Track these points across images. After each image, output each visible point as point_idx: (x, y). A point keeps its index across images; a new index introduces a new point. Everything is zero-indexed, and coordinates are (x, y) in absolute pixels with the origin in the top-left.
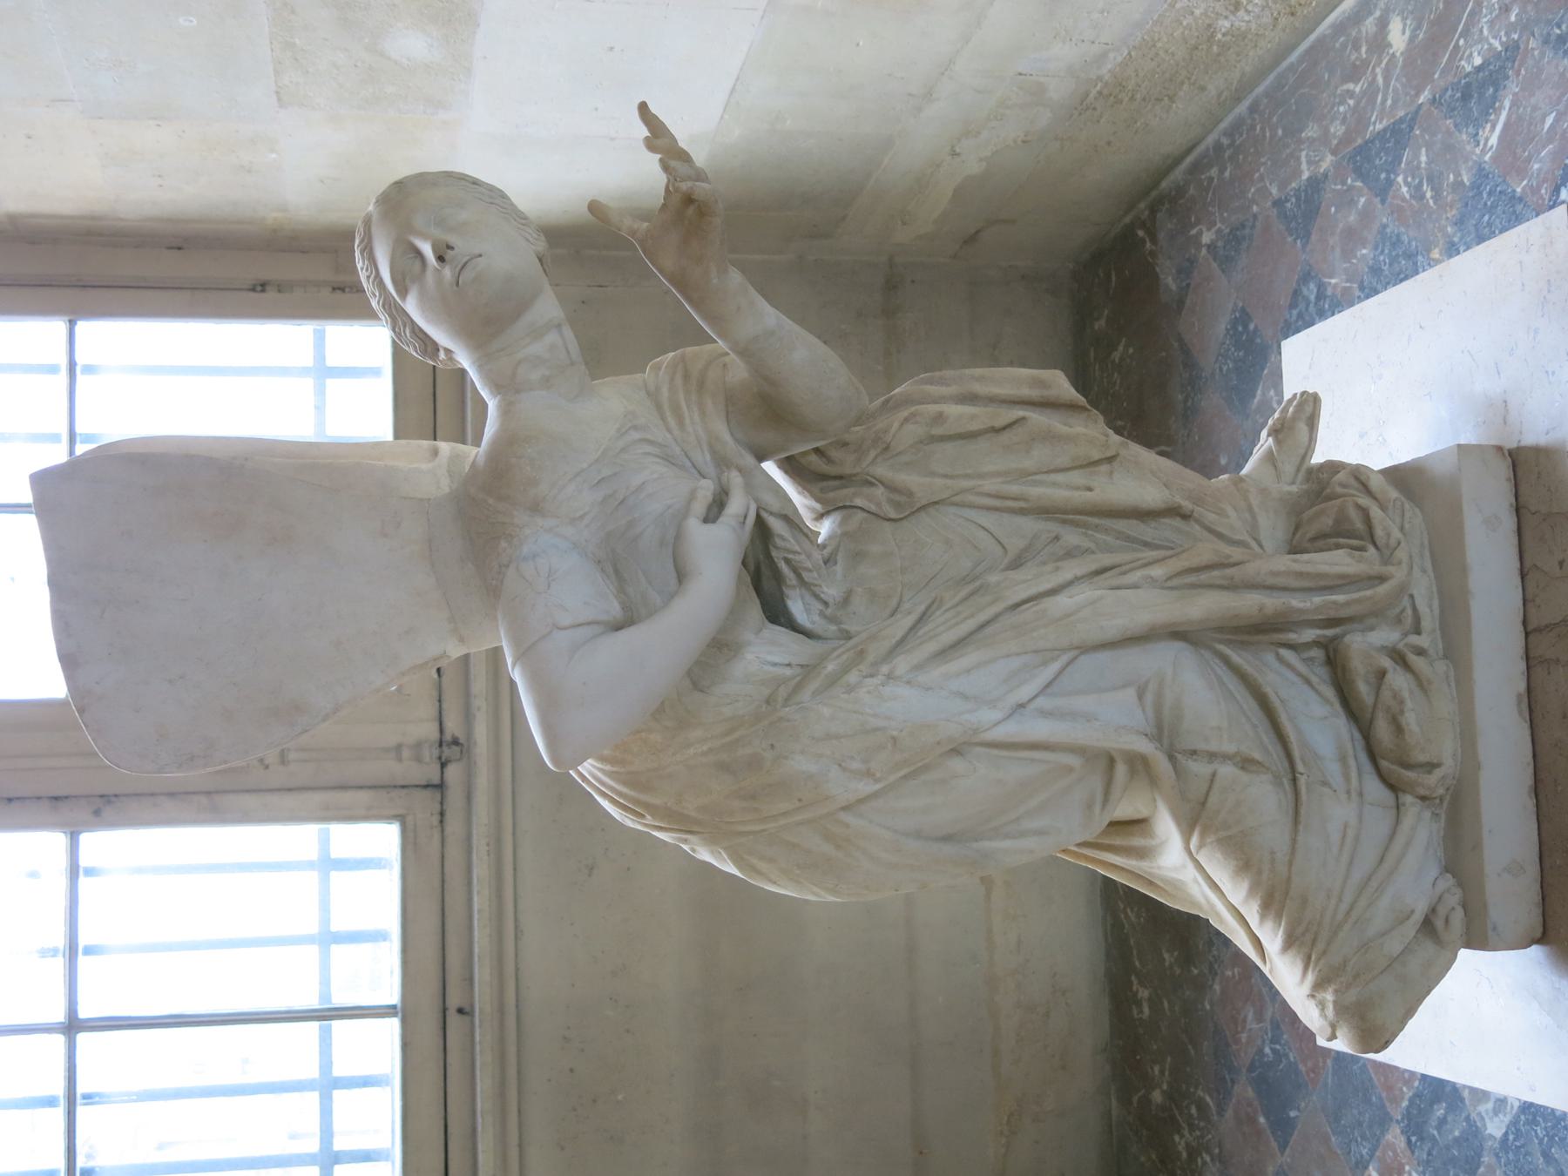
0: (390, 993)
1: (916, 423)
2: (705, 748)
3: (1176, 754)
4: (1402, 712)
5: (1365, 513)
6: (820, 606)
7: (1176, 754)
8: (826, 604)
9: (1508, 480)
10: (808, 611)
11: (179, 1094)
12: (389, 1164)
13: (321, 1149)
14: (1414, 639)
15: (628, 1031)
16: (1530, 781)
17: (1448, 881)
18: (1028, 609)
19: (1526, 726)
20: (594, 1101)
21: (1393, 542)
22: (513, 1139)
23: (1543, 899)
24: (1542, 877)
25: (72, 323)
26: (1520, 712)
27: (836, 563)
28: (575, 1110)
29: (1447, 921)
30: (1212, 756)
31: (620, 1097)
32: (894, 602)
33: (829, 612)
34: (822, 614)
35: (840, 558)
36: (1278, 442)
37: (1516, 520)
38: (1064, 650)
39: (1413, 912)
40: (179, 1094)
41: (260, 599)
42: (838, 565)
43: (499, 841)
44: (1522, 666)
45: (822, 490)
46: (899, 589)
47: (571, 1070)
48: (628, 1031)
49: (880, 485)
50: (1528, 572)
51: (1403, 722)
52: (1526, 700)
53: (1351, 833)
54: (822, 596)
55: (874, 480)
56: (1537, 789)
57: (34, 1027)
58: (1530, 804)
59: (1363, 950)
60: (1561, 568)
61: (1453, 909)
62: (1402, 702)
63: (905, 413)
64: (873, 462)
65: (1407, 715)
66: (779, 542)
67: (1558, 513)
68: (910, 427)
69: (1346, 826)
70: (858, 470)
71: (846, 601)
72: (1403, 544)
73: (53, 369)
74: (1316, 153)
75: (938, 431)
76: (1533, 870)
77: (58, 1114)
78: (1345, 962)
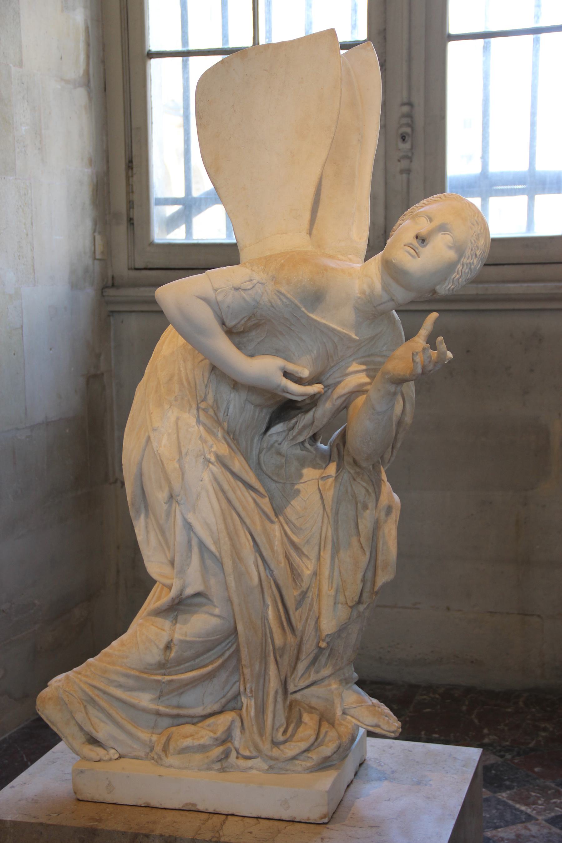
1: (365, 496)
2: (182, 369)
3: (177, 613)
6: (280, 440)
7: (177, 613)
8: (280, 444)
9: (308, 819)
10: (278, 433)
13: (195, 199)
14: (234, 754)
18: (247, 539)
23: (95, 802)
24: (106, 803)
26: (187, 804)
27: (302, 450)
32: (275, 478)
33: (276, 445)
34: (277, 441)
38: (220, 553)
41: (266, 149)
45: (338, 445)
46: (282, 481)
49: (336, 475)
50: (258, 820)
52: (193, 809)
54: (284, 441)
55: (339, 472)
57: (256, 24)
60: (248, 832)
63: (370, 490)
64: (349, 472)
66: (303, 417)
67: (278, 835)
68: (363, 491)
70: (345, 463)
71: (279, 453)
75: (359, 506)
76: (109, 798)
77: (179, 47)
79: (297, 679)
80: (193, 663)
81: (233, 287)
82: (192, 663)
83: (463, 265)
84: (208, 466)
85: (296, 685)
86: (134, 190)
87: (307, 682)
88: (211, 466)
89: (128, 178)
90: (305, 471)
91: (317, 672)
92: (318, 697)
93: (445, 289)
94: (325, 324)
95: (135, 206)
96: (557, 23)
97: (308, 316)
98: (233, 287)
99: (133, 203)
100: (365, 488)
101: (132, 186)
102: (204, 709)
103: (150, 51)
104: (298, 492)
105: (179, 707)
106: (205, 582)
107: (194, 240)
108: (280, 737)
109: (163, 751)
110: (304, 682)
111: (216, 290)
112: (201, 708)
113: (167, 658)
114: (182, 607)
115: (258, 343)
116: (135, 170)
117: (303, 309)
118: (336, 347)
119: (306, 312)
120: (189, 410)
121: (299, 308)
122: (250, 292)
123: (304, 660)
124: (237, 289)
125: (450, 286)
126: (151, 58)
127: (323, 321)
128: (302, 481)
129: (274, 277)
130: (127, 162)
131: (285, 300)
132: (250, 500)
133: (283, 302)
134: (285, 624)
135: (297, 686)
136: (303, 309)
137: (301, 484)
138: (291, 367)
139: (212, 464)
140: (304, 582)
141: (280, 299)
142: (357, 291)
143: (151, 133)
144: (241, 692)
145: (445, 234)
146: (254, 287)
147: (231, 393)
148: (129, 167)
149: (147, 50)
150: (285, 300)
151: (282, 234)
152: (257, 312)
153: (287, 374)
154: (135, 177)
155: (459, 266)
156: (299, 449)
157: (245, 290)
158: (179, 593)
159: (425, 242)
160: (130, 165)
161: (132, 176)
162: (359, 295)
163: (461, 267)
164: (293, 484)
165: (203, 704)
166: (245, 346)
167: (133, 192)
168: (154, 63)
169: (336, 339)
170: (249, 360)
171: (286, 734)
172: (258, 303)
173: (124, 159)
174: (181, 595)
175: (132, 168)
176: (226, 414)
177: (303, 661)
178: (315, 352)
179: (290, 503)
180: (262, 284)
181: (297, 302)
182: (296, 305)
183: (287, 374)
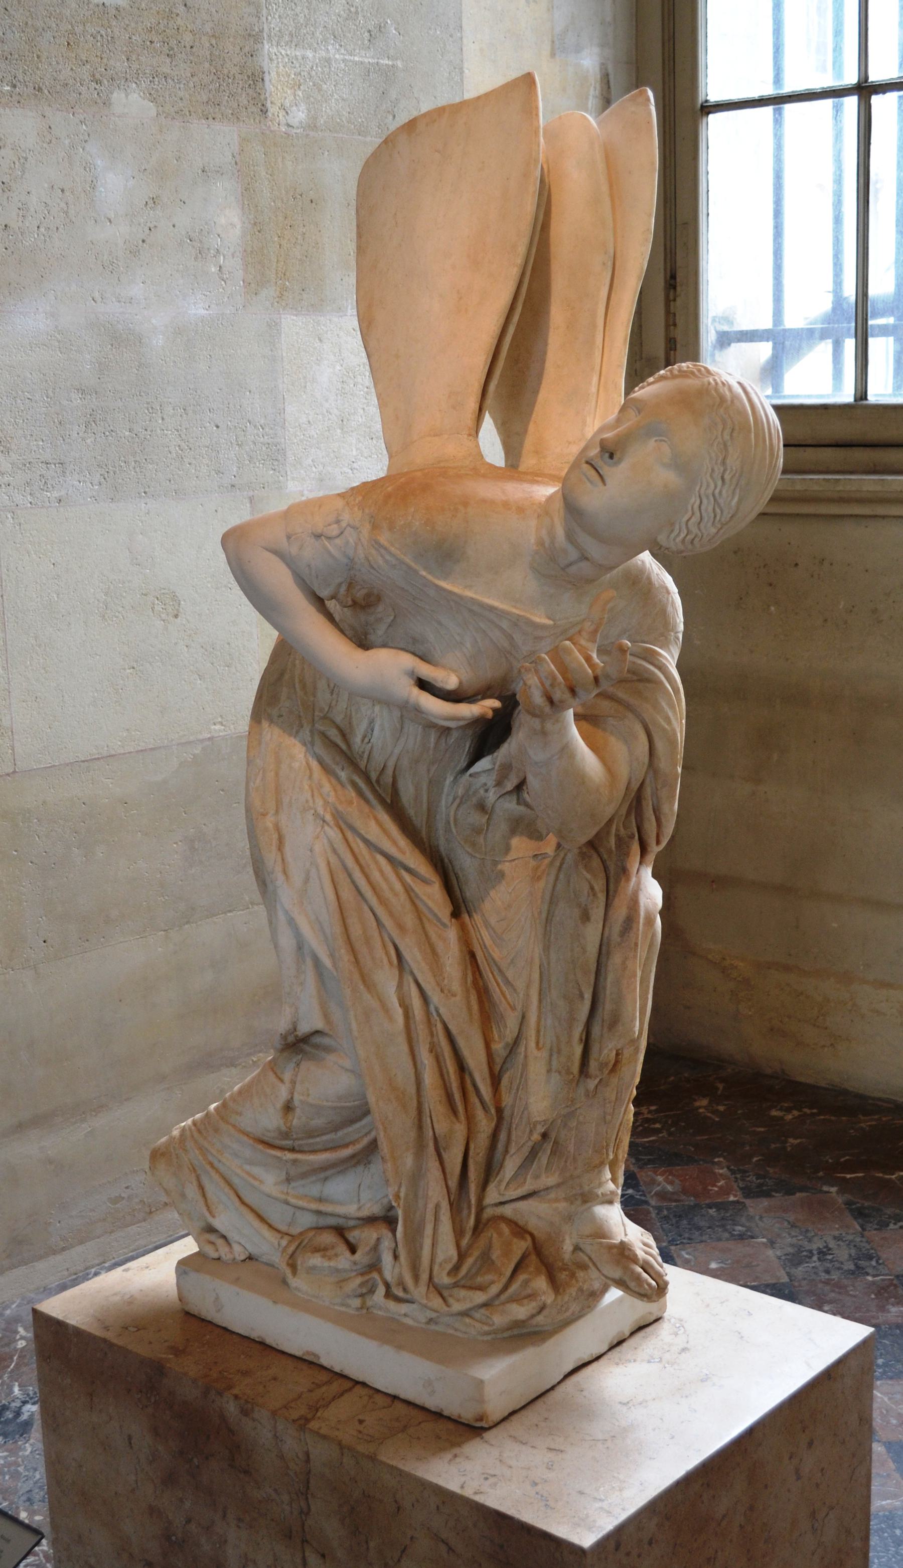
0: (874, 397)
1: (589, 896)
4: (323, 1256)
5: (481, 1288)
11: (778, 213)
12: (890, 390)
15: (826, 620)
16: (269, 1341)
17: (239, 1253)
19: (298, 1353)
20: (771, 585)
21: (451, 1300)
22: (823, 509)
25: (709, 109)
28: (765, 566)
29: (213, 1243)
30: (293, 1083)
31: (773, 608)
35: (522, 808)
36: (611, 1247)
37: (433, 1409)
39: (214, 1217)
40: (778, 213)
42: (516, 806)
43: (842, 500)
44: (337, 1369)
47: (796, 565)
48: (826, 620)
51: (318, 1255)
53: (256, 1183)
56: (225, 1329)
58: (254, 1335)
59: (190, 1166)
61: (217, 1250)
62: (330, 1259)
65: (319, 1259)
69: (261, 1182)
72: (446, 1308)
73: (778, 80)
74: (148, 1173)
77: (768, 90)
78: (186, 1150)
79: (504, 1184)
80: (334, 1137)
81: (312, 533)
82: (332, 1136)
83: (700, 496)
84: (323, 827)
85: (502, 1193)
86: (677, 321)
87: (520, 1192)
88: (326, 828)
89: (668, 301)
90: (515, 841)
91: (537, 1177)
92: (539, 1217)
93: (674, 540)
94: (472, 599)
95: (678, 346)
96: (770, 5)
97: (437, 586)
98: (312, 533)
99: (675, 341)
100: (590, 883)
101: (675, 314)
102: (359, 1209)
103: (707, 101)
104: (502, 875)
105: (320, 1200)
106: (326, 1016)
107: (784, 397)
108: (444, 1279)
109: (288, 1264)
110: (515, 1189)
111: (289, 537)
112: (355, 1206)
113: (288, 1125)
114: (307, 1048)
115: (390, 626)
116: (678, 289)
117: (424, 573)
118: (510, 638)
119: (430, 577)
120: (297, 732)
121: (416, 572)
122: (338, 541)
123: (514, 1154)
124: (318, 536)
125: (682, 535)
126: (708, 113)
127: (469, 594)
128: (509, 858)
129: (372, 517)
130: (668, 278)
131: (388, 557)
132: (398, 886)
133: (386, 561)
134: (457, 1096)
135: (503, 1195)
136: (424, 573)
137: (507, 864)
138: (426, 671)
139: (328, 824)
140: (508, 1029)
141: (382, 556)
142: (533, 541)
143: (705, 231)
144: (518, 1164)
145: (661, 441)
146: (342, 533)
147: (374, 705)
148: (671, 285)
149: (701, 99)
150: (388, 557)
151: (434, 436)
152: (355, 576)
153: (423, 685)
154: (679, 301)
155: (692, 500)
156: (515, 802)
157: (329, 538)
158: (291, 1026)
159: (616, 457)
160: (672, 282)
161: (675, 300)
162: (535, 547)
163: (698, 502)
164: (495, 863)
165: (359, 1200)
166: (374, 629)
167: (675, 325)
168: (713, 119)
169: (505, 625)
170: (360, 655)
171: (456, 1275)
172: (352, 560)
173: (662, 275)
174: (295, 1030)
175: (675, 288)
176: (366, 740)
177: (514, 1157)
178: (468, 645)
179: (489, 894)
180: (353, 527)
181: (408, 560)
182: (409, 567)
183: (423, 685)
